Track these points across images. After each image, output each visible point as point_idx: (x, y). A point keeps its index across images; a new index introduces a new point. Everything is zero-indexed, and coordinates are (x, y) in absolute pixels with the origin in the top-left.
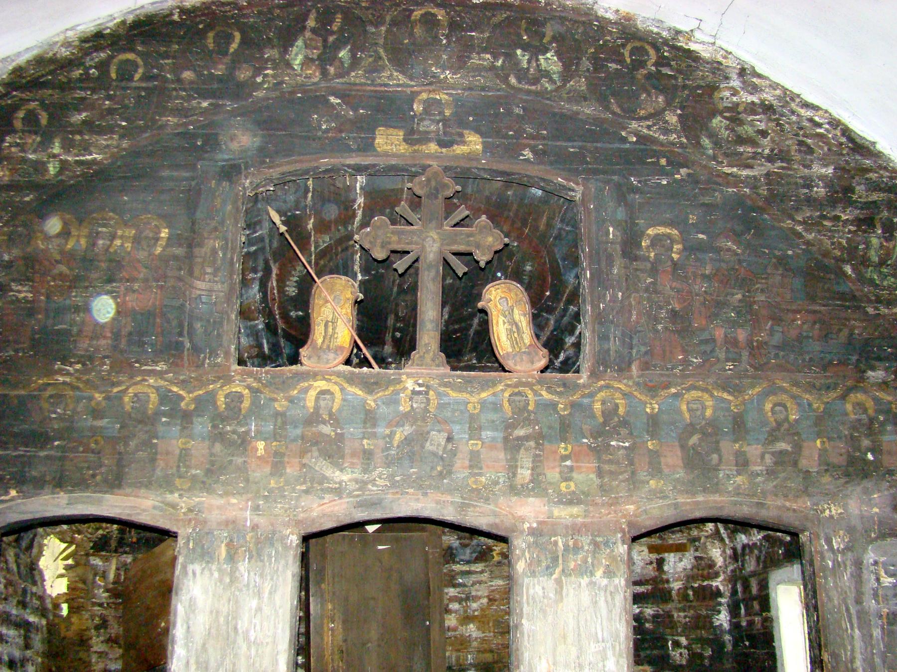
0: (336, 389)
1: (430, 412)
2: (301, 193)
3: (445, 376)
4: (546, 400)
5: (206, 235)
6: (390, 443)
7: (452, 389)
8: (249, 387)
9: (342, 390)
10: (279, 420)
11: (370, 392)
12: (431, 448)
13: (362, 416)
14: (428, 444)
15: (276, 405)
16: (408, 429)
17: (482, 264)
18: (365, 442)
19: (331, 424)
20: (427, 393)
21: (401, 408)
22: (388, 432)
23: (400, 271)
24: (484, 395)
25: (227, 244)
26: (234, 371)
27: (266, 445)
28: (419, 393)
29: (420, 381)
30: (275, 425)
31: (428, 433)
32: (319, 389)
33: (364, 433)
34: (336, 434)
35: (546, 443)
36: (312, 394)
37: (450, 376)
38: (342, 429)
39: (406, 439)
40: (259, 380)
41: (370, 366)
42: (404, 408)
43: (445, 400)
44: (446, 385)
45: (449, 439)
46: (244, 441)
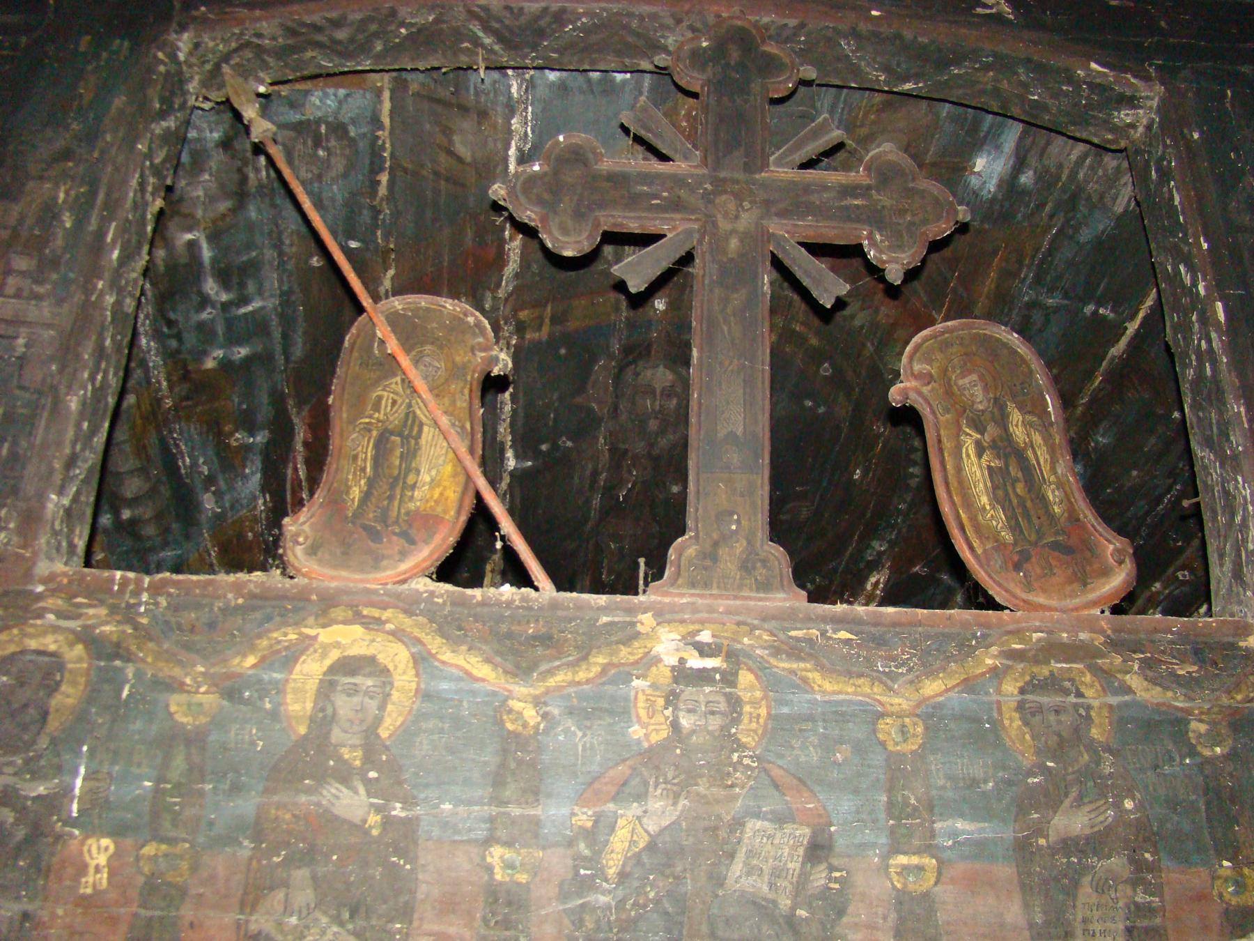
0: (396, 656)
1: (742, 747)
2: (359, 177)
3: (789, 618)
4: (1143, 706)
5: (33, 168)
6: (593, 860)
7: (820, 667)
8: (88, 638)
9: (422, 660)
10: (179, 762)
11: (522, 669)
12: (748, 884)
13: (489, 757)
14: (737, 867)
15: (176, 703)
16: (658, 813)
17: (894, 275)
18: (496, 854)
19: (367, 782)
20: (729, 678)
21: (636, 732)
22: (584, 818)
23: (636, 285)
24: (932, 687)
25: (93, 194)
26: (49, 579)
27: (117, 855)
28: (703, 676)
29: (705, 637)
30: (159, 780)
31: (738, 823)
32: (335, 655)
33: (491, 820)
34: (388, 822)
35: (1166, 863)
36: (311, 669)
37: (809, 620)
38: (408, 802)
39: (651, 847)
40: (128, 615)
41: (522, 578)
42: (646, 729)
43: (799, 702)
44: (794, 651)
45: (818, 850)
46: (37, 832)
